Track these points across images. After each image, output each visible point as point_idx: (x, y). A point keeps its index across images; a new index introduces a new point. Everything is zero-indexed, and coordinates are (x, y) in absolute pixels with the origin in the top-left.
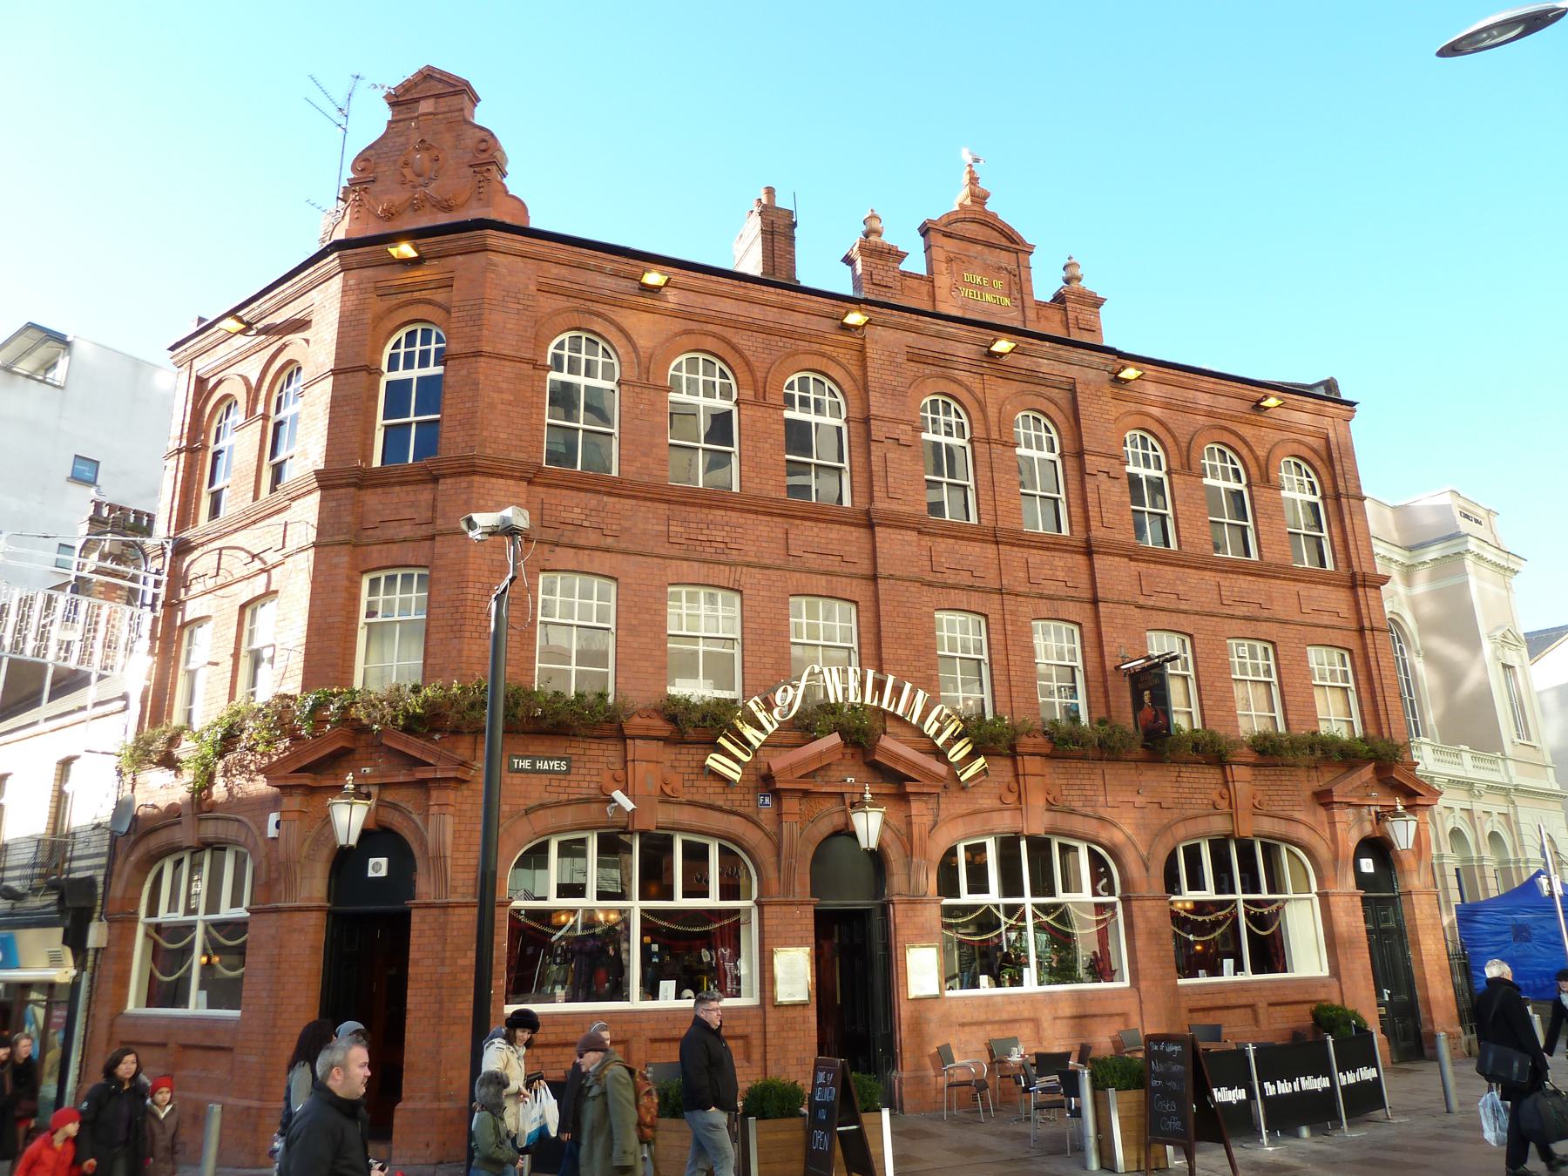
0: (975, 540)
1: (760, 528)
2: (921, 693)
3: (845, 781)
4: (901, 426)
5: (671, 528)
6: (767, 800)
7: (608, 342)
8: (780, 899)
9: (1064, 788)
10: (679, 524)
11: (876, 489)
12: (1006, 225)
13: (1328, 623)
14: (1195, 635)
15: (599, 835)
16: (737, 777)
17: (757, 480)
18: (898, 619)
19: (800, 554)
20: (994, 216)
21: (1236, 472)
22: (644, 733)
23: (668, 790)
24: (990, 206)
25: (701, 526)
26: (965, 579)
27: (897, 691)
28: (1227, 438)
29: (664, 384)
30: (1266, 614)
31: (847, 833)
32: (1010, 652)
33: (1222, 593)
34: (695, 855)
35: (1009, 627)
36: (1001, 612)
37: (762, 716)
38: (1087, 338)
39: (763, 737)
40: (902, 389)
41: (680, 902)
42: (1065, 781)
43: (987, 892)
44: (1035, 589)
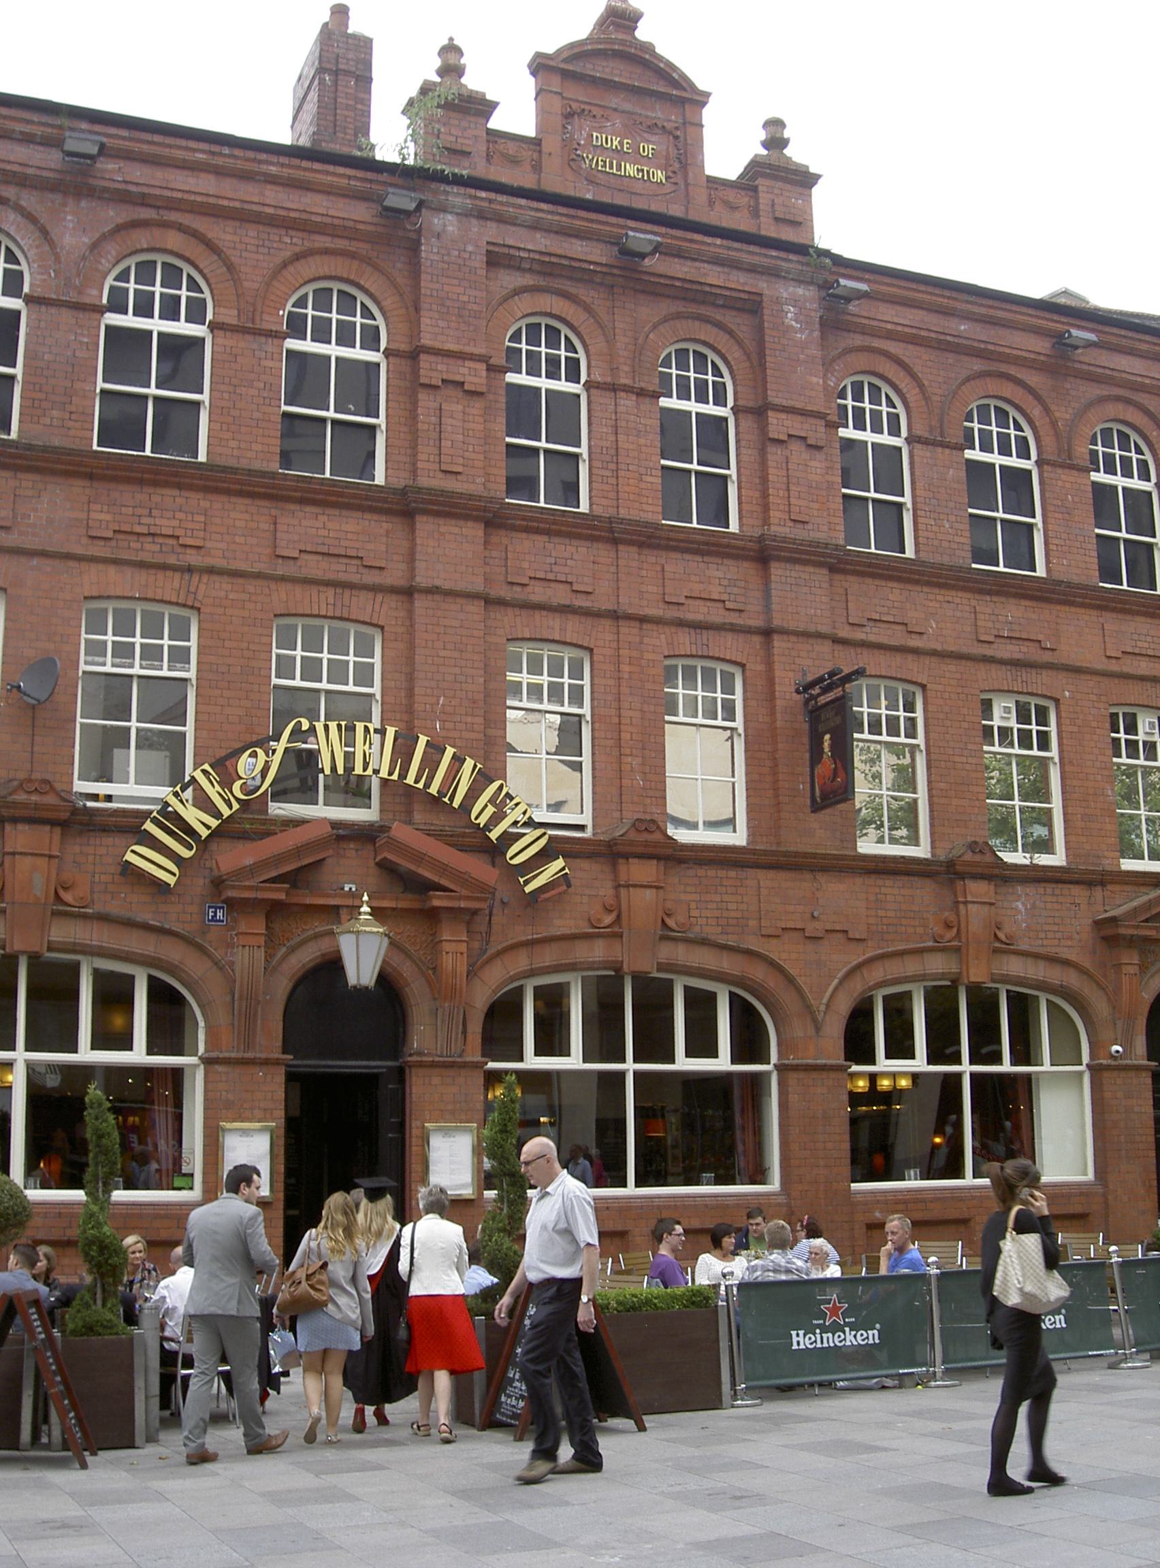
0: (578, 537)
1: (232, 514)
2: (469, 763)
3: (343, 889)
4: (467, 363)
5: (93, 515)
6: (219, 914)
7: (196, 267)
8: (233, 1055)
9: (693, 905)
10: (105, 508)
11: (421, 456)
12: (670, 64)
13: (1146, 673)
14: (929, 686)
15: (583, 978)
16: (171, 880)
17: (233, 444)
18: (442, 653)
19: (296, 554)
20: (648, 48)
21: (1143, 465)
22: (640, 850)
23: (670, 922)
24: (643, 33)
25: (139, 511)
26: (560, 595)
27: (430, 763)
28: (1008, 390)
29: (278, 328)
30: (1047, 657)
31: (333, 965)
32: (625, 705)
33: (979, 623)
34: (701, 1006)
35: (625, 668)
36: (614, 645)
37: (213, 792)
38: (787, 234)
39: (214, 823)
40: (475, 307)
41: (684, 1063)
42: (696, 897)
43: (913, 1057)
44: (672, 613)
